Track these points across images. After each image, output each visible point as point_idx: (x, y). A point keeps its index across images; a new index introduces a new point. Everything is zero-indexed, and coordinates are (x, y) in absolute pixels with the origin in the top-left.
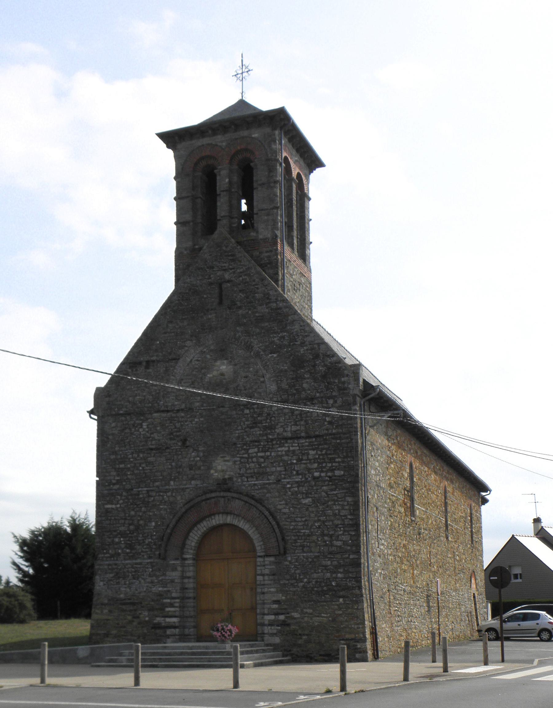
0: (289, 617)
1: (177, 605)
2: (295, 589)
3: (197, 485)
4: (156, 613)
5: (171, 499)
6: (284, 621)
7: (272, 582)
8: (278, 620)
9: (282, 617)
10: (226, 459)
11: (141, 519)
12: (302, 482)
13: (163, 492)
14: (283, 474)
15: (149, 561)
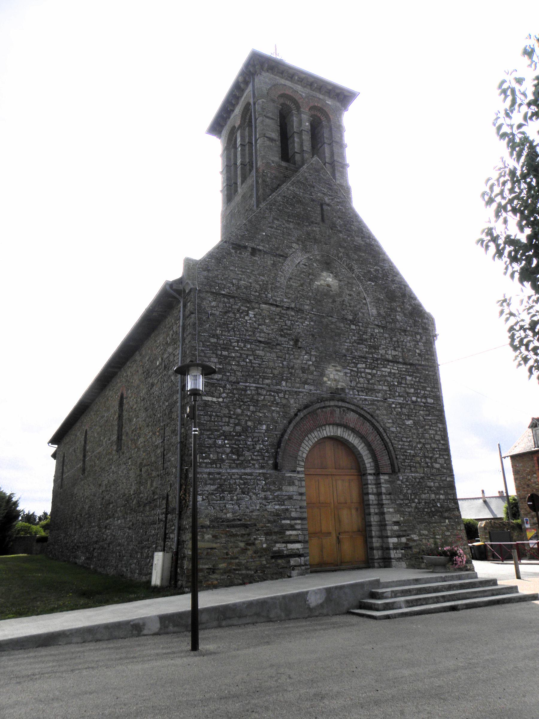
2: (409, 510)
3: (311, 390)
5: (284, 401)
6: (406, 544)
9: (404, 540)
11: (250, 420)
12: (403, 404)
15: (261, 471)
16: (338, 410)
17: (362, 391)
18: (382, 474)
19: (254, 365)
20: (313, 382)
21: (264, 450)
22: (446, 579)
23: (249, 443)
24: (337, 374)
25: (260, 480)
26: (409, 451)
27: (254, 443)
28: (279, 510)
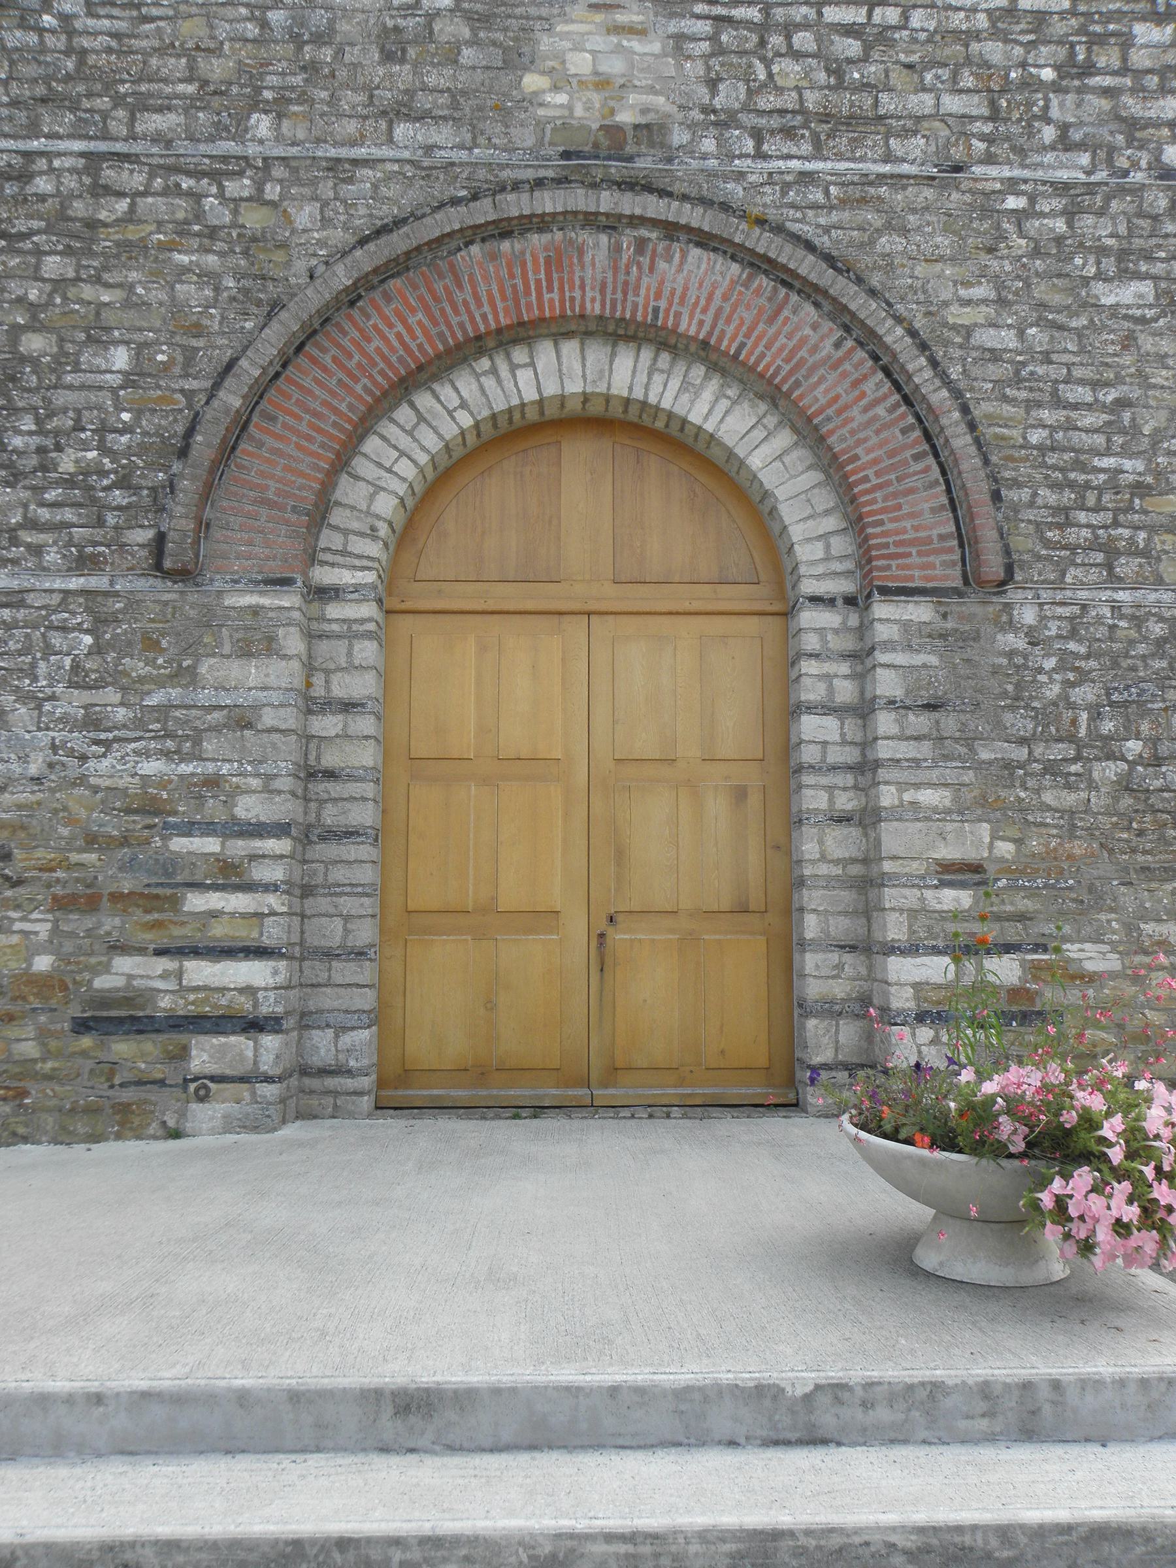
0: (1049, 967)
1: (274, 873)
2: (1070, 799)
3: (429, 149)
4: (110, 923)
5: (254, 219)
6: (1015, 993)
7: (925, 749)
8: (981, 987)
9: (1005, 970)
10: (621, 18)
11: (35, 326)
12: (1091, 189)
13: (197, 174)
14: (983, 138)
15: (75, 583)
16: (598, 245)
17: (789, 133)
18: (884, 591)
19: (86, 43)
20: (455, 105)
21: (103, 473)
22: (827, 1419)
23: (18, 442)
24: (619, 49)
25: (64, 629)
26: (1108, 462)
27: (49, 442)
28: (163, 784)
